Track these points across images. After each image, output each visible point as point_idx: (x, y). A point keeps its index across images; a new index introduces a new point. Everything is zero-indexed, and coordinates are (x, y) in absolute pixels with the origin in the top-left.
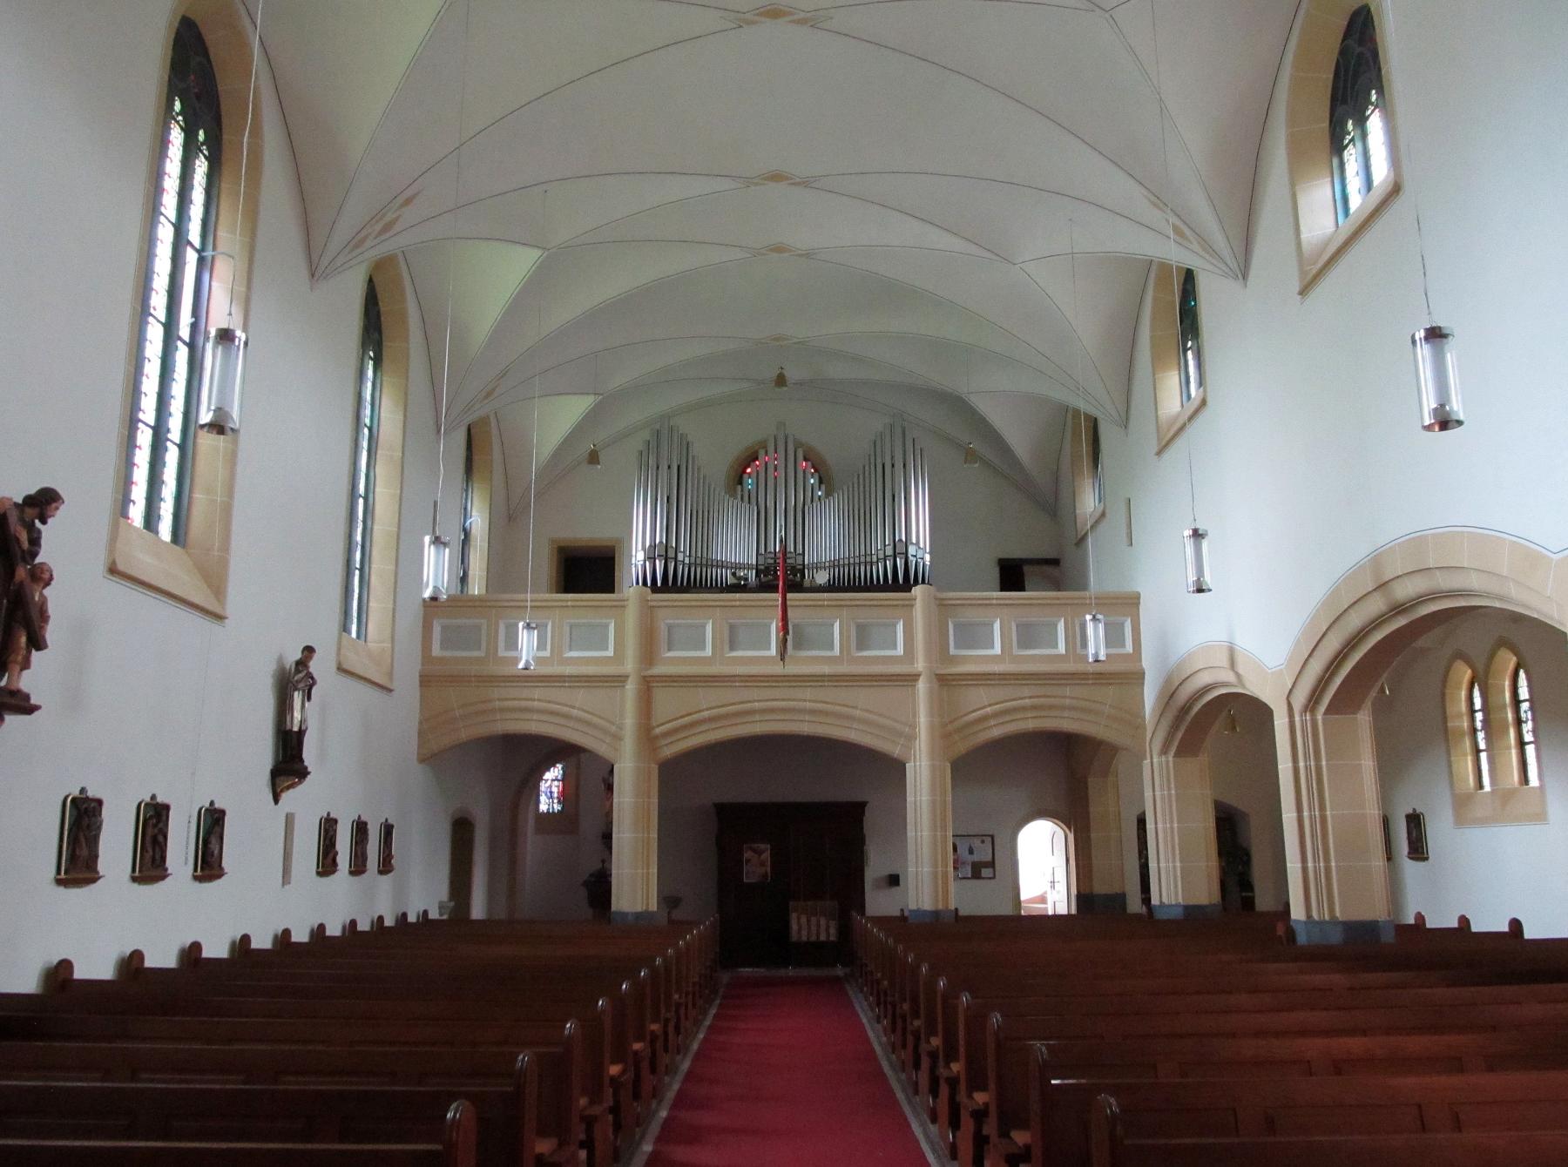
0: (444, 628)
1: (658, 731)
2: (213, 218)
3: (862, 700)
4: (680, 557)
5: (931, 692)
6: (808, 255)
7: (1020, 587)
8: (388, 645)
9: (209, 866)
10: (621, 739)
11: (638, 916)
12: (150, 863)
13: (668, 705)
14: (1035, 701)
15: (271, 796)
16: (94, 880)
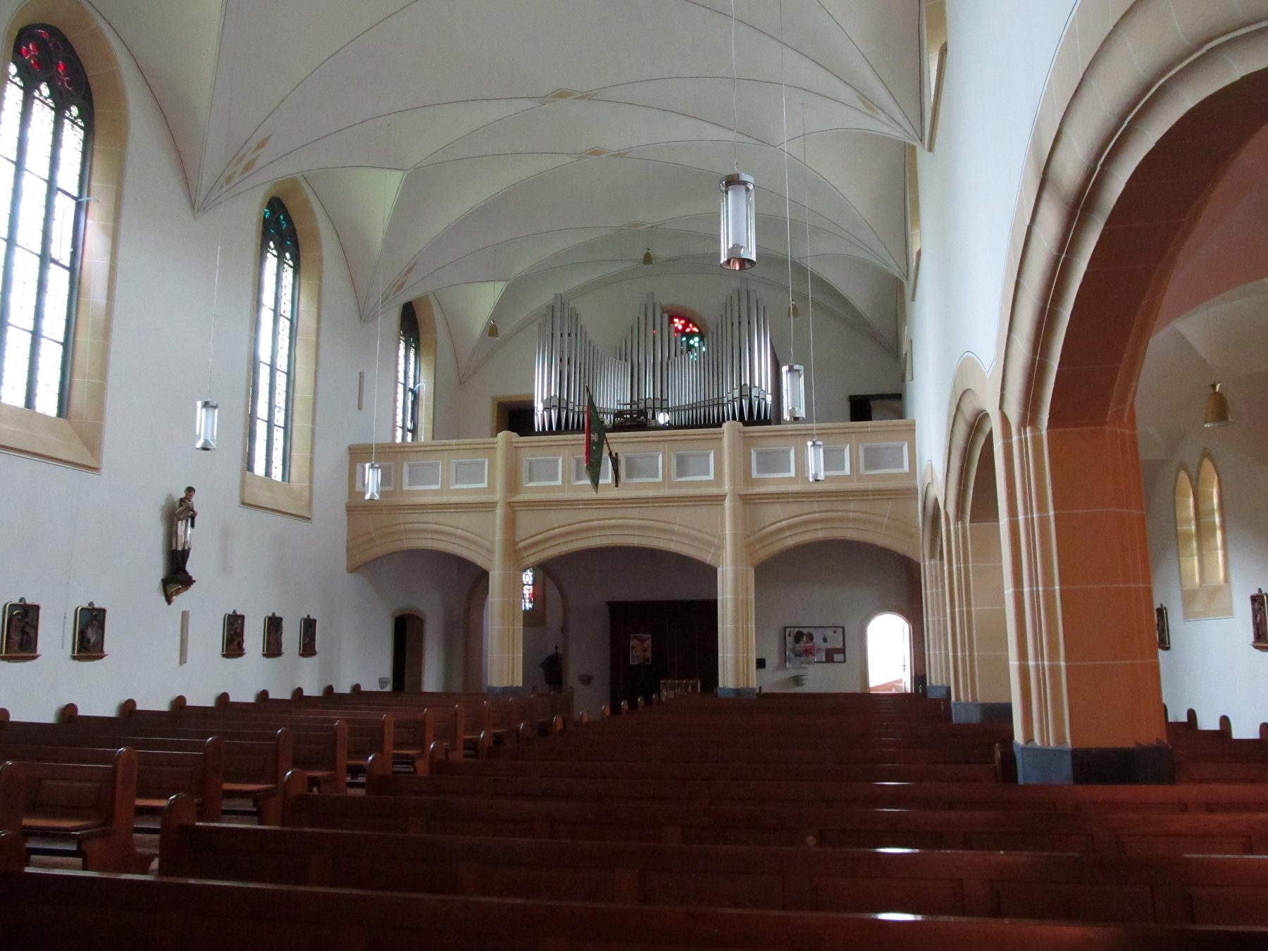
1: (520, 545)
2: (87, 173)
3: (682, 517)
4: (571, 406)
5: (734, 509)
6: (620, 155)
7: (867, 417)
8: (307, 484)
9: (308, 649)
10: (493, 552)
11: (504, 689)
12: (273, 648)
13: (529, 525)
14: (824, 515)
15: (163, 598)
16: (101, 657)
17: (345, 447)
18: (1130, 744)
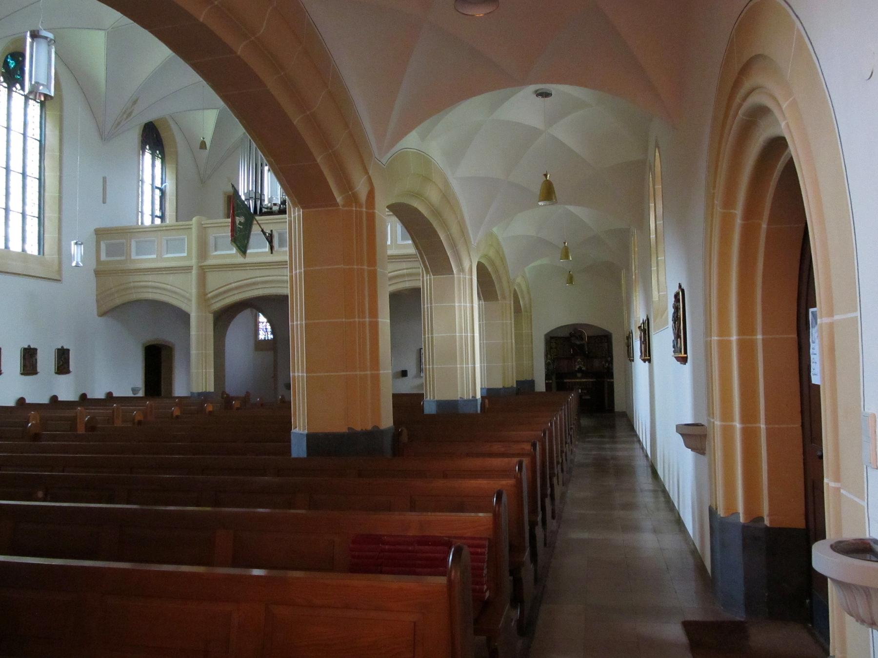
0: (107, 246)
1: (209, 295)
11: (200, 394)
13: (215, 281)
17: (92, 230)
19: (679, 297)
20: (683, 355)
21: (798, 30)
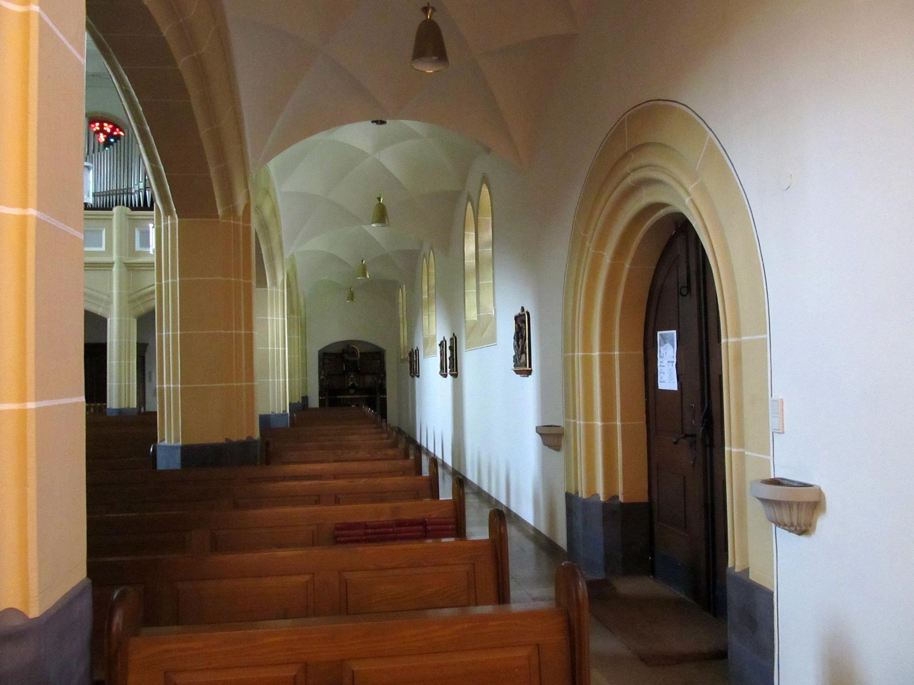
17: (381, 344)
18: (220, 440)
19: (521, 321)
20: (528, 368)
21: (710, 139)
